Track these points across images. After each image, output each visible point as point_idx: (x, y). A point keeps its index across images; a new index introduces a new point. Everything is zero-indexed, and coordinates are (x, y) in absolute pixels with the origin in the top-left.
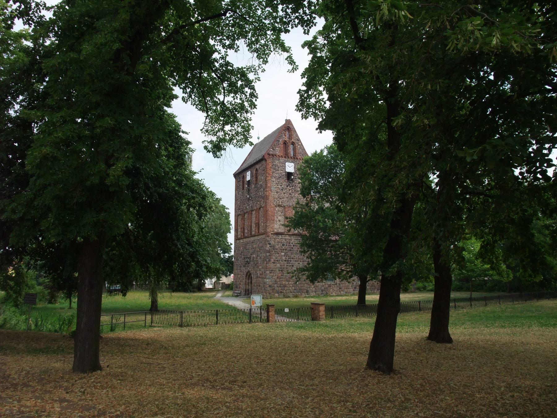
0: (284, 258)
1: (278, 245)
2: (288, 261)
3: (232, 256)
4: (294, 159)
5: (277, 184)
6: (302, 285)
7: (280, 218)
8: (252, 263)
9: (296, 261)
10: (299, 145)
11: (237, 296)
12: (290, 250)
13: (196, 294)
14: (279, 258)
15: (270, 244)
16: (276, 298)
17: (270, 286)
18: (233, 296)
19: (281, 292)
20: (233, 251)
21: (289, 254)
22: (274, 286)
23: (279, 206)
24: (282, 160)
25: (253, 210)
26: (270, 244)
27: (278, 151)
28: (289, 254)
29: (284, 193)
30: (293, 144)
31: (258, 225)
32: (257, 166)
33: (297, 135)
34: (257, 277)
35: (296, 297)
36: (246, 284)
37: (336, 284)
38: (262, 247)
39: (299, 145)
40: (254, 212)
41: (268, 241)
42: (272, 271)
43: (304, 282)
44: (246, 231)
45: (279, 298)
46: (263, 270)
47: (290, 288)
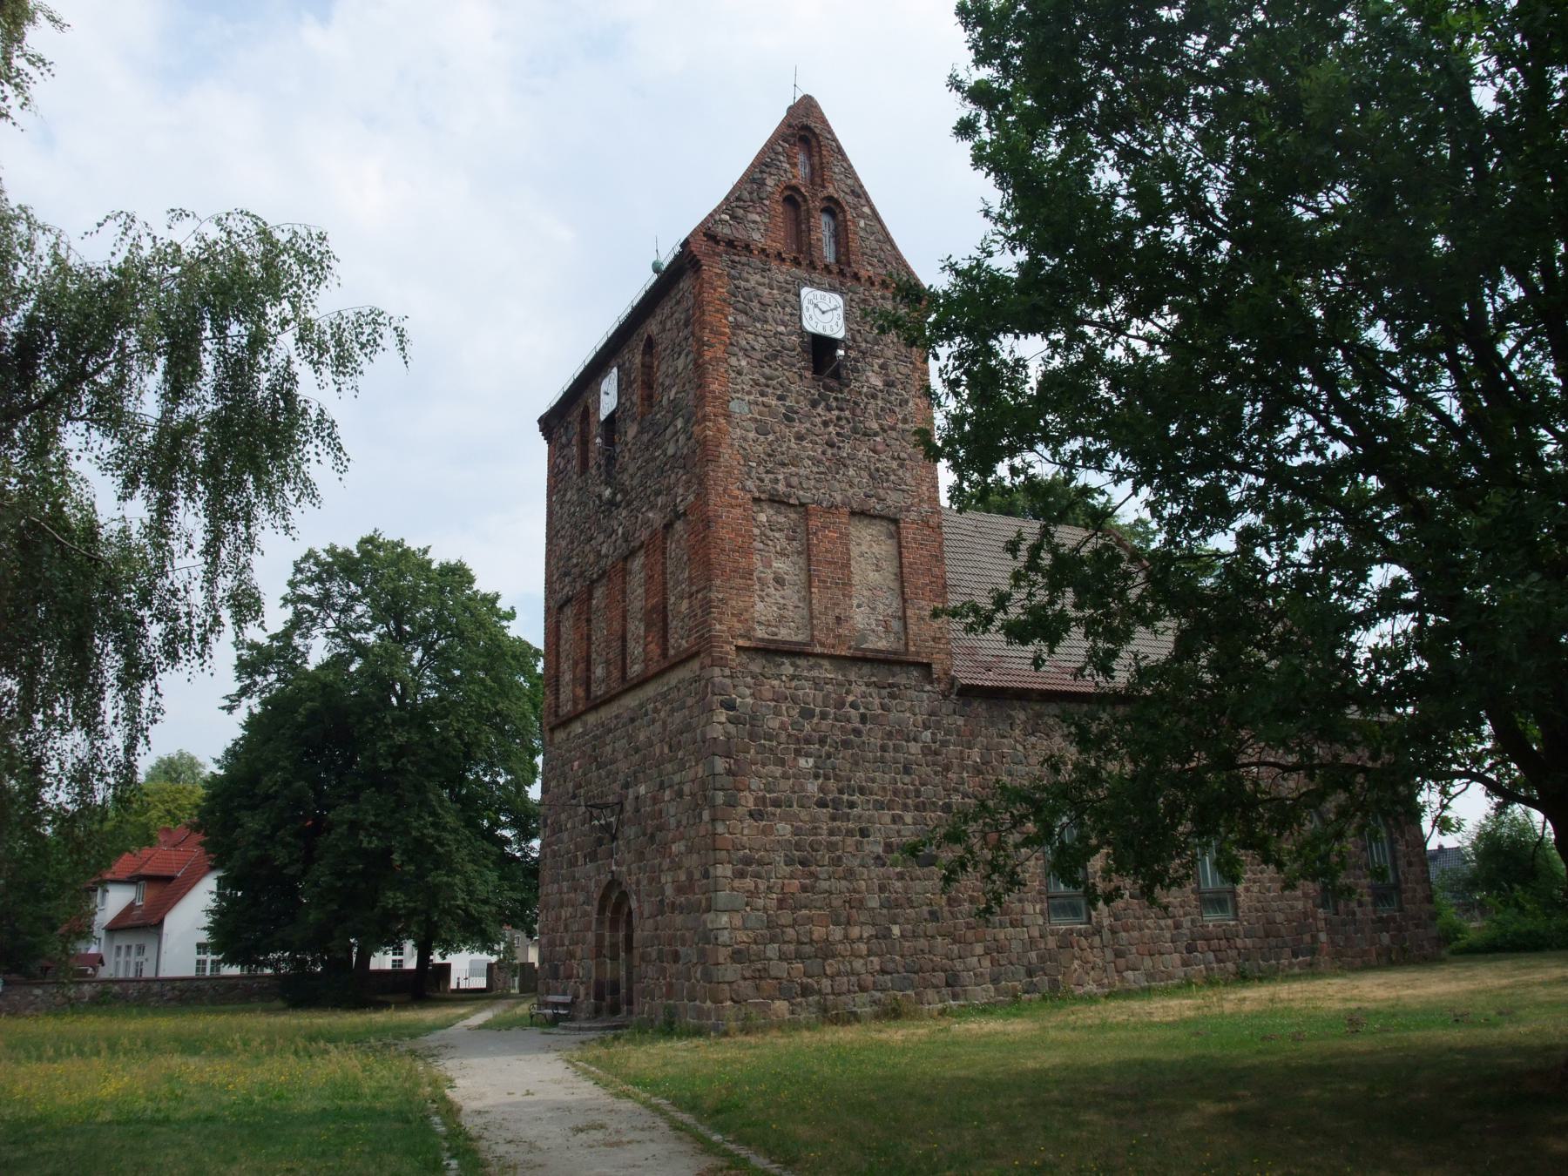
0: (812, 787)
1: (777, 713)
2: (836, 804)
4: (841, 275)
5: (761, 387)
6: (922, 943)
7: (780, 565)
8: (631, 831)
9: (880, 806)
10: (862, 216)
11: (555, 1021)
12: (846, 744)
13: (380, 1018)
14: (785, 785)
15: (729, 706)
17: (737, 956)
18: (532, 1021)
19: (806, 991)
21: (842, 761)
22: (761, 957)
23: (777, 501)
24: (781, 273)
25: (632, 553)
26: (729, 706)
27: (759, 230)
28: (842, 761)
29: (799, 437)
30: (832, 208)
31: (659, 617)
32: (652, 327)
33: (849, 171)
34: (661, 908)
35: (893, 1013)
36: (599, 954)
37: (1098, 931)
38: (687, 728)
39: (862, 216)
40: (637, 564)
41: (723, 690)
42: (747, 861)
43: (931, 927)
44: (599, 671)
45: (795, 1026)
46: (692, 861)
47: (858, 964)
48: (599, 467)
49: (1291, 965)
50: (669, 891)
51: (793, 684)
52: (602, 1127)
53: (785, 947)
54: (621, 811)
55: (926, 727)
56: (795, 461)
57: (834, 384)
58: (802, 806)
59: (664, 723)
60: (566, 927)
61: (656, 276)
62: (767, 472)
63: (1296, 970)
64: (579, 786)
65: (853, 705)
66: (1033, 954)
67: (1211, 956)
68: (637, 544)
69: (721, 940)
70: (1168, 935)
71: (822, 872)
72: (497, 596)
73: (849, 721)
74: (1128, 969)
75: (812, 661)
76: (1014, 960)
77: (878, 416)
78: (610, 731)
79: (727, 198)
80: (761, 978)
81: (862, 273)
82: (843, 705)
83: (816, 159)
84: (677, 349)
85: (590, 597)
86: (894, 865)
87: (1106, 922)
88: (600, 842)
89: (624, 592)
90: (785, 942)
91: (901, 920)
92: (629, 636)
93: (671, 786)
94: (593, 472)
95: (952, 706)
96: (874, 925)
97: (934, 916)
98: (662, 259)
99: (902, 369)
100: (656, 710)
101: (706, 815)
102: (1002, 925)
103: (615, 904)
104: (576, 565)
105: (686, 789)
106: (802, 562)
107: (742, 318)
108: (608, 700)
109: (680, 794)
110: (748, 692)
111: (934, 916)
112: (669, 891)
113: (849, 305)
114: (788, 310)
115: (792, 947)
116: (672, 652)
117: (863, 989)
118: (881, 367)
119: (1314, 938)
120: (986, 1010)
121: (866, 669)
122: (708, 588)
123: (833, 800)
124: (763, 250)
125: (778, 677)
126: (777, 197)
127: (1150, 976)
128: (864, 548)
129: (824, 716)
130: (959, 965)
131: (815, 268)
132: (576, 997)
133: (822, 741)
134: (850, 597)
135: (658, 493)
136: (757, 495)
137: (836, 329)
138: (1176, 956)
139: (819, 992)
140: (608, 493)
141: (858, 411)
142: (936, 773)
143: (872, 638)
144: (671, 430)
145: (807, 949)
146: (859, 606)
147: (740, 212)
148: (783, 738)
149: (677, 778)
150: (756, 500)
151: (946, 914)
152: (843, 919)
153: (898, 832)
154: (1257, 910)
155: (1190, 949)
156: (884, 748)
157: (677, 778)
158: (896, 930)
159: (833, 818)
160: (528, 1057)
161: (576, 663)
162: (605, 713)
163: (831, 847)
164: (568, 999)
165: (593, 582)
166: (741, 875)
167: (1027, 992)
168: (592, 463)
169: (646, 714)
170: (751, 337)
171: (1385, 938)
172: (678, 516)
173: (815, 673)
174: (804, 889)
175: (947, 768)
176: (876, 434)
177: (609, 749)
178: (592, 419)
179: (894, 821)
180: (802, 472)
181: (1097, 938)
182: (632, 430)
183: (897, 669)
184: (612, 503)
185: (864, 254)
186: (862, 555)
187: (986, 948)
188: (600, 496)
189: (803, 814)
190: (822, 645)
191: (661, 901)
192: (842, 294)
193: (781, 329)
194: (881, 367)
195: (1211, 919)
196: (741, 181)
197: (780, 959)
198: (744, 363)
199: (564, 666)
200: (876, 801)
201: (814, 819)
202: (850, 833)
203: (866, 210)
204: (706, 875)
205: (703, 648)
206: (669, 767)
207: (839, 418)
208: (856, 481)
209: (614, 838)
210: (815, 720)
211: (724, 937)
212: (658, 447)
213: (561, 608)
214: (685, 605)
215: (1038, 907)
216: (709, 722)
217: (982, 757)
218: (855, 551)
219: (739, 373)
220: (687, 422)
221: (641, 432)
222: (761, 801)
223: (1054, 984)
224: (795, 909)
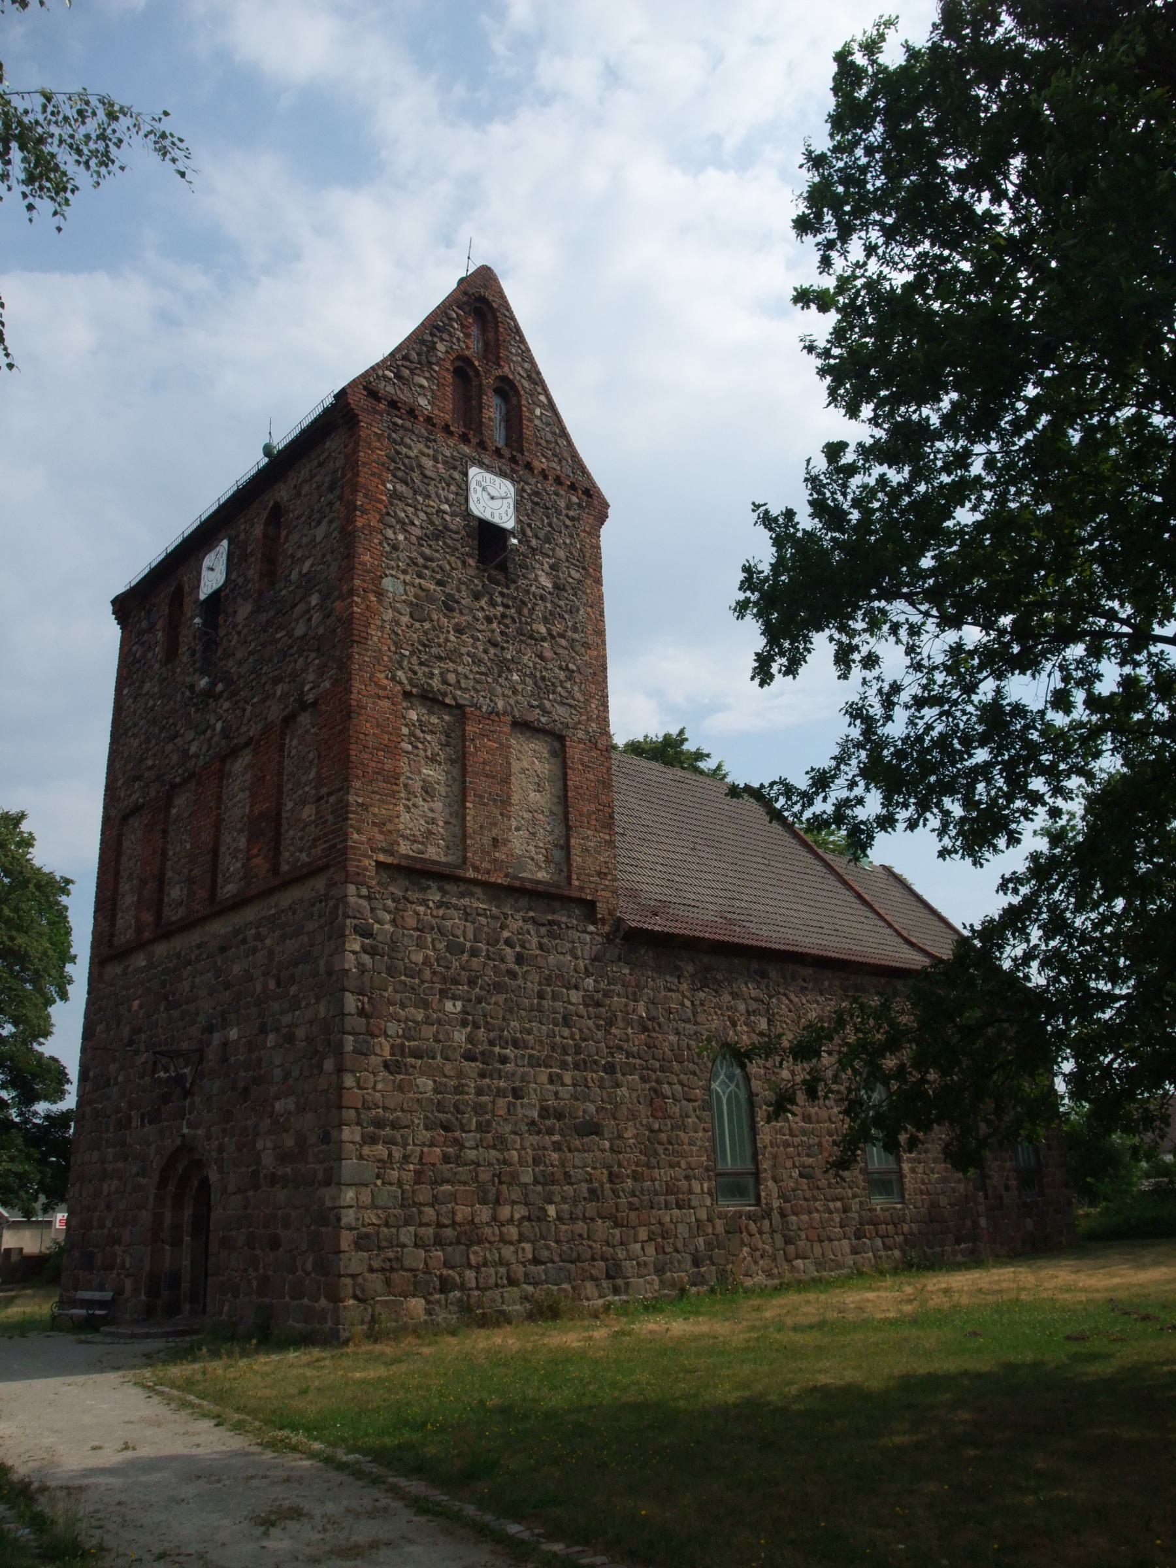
0: (460, 1036)
2: (486, 1057)
3: (65, 1117)
4: (512, 459)
9: (534, 1062)
11: (89, 1325)
12: (499, 987)
14: (428, 1031)
15: (366, 933)
16: (416, 1331)
17: (362, 1242)
18: (55, 1325)
19: (445, 1286)
20: (72, 1089)
23: (429, 699)
24: (448, 447)
25: (234, 752)
26: (366, 933)
27: (428, 396)
30: (507, 390)
31: (268, 827)
35: (547, 1312)
37: (767, 1214)
40: (238, 766)
42: (379, 1123)
43: (591, 1208)
44: (176, 893)
47: (508, 1252)
48: (193, 654)
49: (954, 1253)
50: (268, 1159)
51: (441, 912)
52: (296, 1513)
53: (422, 1230)
54: (201, 1061)
55: (588, 974)
56: (454, 656)
57: (501, 577)
58: (447, 1059)
59: (271, 954)
60: (109, 1207)
61: (266, 460)
62: (421, 664)
63: (959, 1258)
64: (138, 1031)
65: (508, 942)
66: (701, 1239)
67: (879, 1242)
68: (243, 740)
69: (344, 1221)
70: (838, 1219)
71: (470, 1139)
72: (22, 816)
73: (503, 960)
74: (797, 1257)
75: (463, 888)
76: (680, 1246)
77: (545, 620)
78: (189, 963)
79: (392, 354)
80: (392, 1269)
81: (536, 463)
82: (497, 941)
83: (491, 335)
84: (316, 516)
85: (169, 805)
86: (550, 1132)
87: (776, 1204)
88: (165, 1099)
89: (219, 798)
90: (421, 1225)
91: (557, 1199)
92: (223, 849)
93: (277, 1030)
94: (185, 659)
95: (617, 951)
96: (526, 1204)
97: (594, 1195)
98: (275, 444)
99: (573, 573)
100: (258, 937)
101: (329, 1065)
102: (667, 1206)
103: (186, 1178)
104: (150, 768)
105: (300, 1033)
106: (456, 772)
107: (401, 488)
108: (187, 926)
109: (290, 1038)
110: (388, 917)
111: (594, 1195)
112: (268, 1159)
113: (520, 492)
114: (453, 488)
115: (431, 1231)
116: (285, 868)
117: (512, 1282)
118: (552, 567)
119: (975, 1224)
120: (652, 1307)
121: (523, 902)
122: (345, 788)
123: (482, 1053)
124: (429, 420)
125: (424, 902)
126: (448, 365)
127: (820, 1266)
128: (525, 764)
129: (474, 953)
130: (621, 1254)
131: (485, 448)
132: (119, 1292)
133: (472, 983)
134: (509, 818)
135: (277, 681)
136: (408, 688)
137: (505, 518)
138: (845, 1242)
139: (462, 1287)
140: (204, 682)
141: (525, 612)
142: (598, 1027)
143: (531, 865)
144: (301, 607)
145: (449, 1232)
146: (518, 829)
147: (406, 373)
148: (427, 974)
149: (286, 1019)
150: (407, 695)
151: (608, 1192)
152: (491, 1196)
153: (556, 1093)
154: (922, 1193)
155: (859, 1235)
156: (541, 995)
157: (286, 1019)
158: (552, 1210)
159: (482, 1075)
160: (81, 1379)
161: (143, 882)
162: (179, 943)
163: (479, 1109)
164: (108, 1295)
165: (174, 787)
166: (372, 1140)
167: (694, 1284)
168: (183, 649)
169: (244, 941)
170: (410, 510)
171: (1029, 1224)
172: (303, 706)
173: (465, 901)
174: (446, 1159)
175: (611, 1022)
176: (543, 639)
177: (186, 985)
178: (187, 600)
179: (551, 1081)
180: (460, 669)
181: (766, 1222)
182: (244, 610)
183: (557, 905)
184: (209, 693)
185: (538, 444)
186: (523, 771)
187: (651, 1232)
188: (192, 687)
189: (448, 1068)
190: (476, 869)
191: (255, 1173)
192: (512, 480)
193: (446, 507)
194: (552, 567)
195: (878, 1202)
196: (409, 338)
197: (416, 1245)
198: (401, 537)
199: (124, 887)
200: (531, 1056)
201: (460, 1074)
202: (500, 1093)
203: (542, 398)
204: (326, 1138)
205: (333, 859)
206: (275, 1006)
207: (504, 616)
208: (520, 687)
209: (187, 1093)
210: (465, 957)
211: (349, 1217)
212: (280, 628)
213: (125, 819)
214: (308, 812)
215: (706, 1186)
216: (340, 950)
217: (648, 1010)
218: (516, 767)
219: (395, 548)
220: (325, 597)
221: (257, 610)
222: (395, 1049)
223: (722, 1275)
224: (435, 1183)
